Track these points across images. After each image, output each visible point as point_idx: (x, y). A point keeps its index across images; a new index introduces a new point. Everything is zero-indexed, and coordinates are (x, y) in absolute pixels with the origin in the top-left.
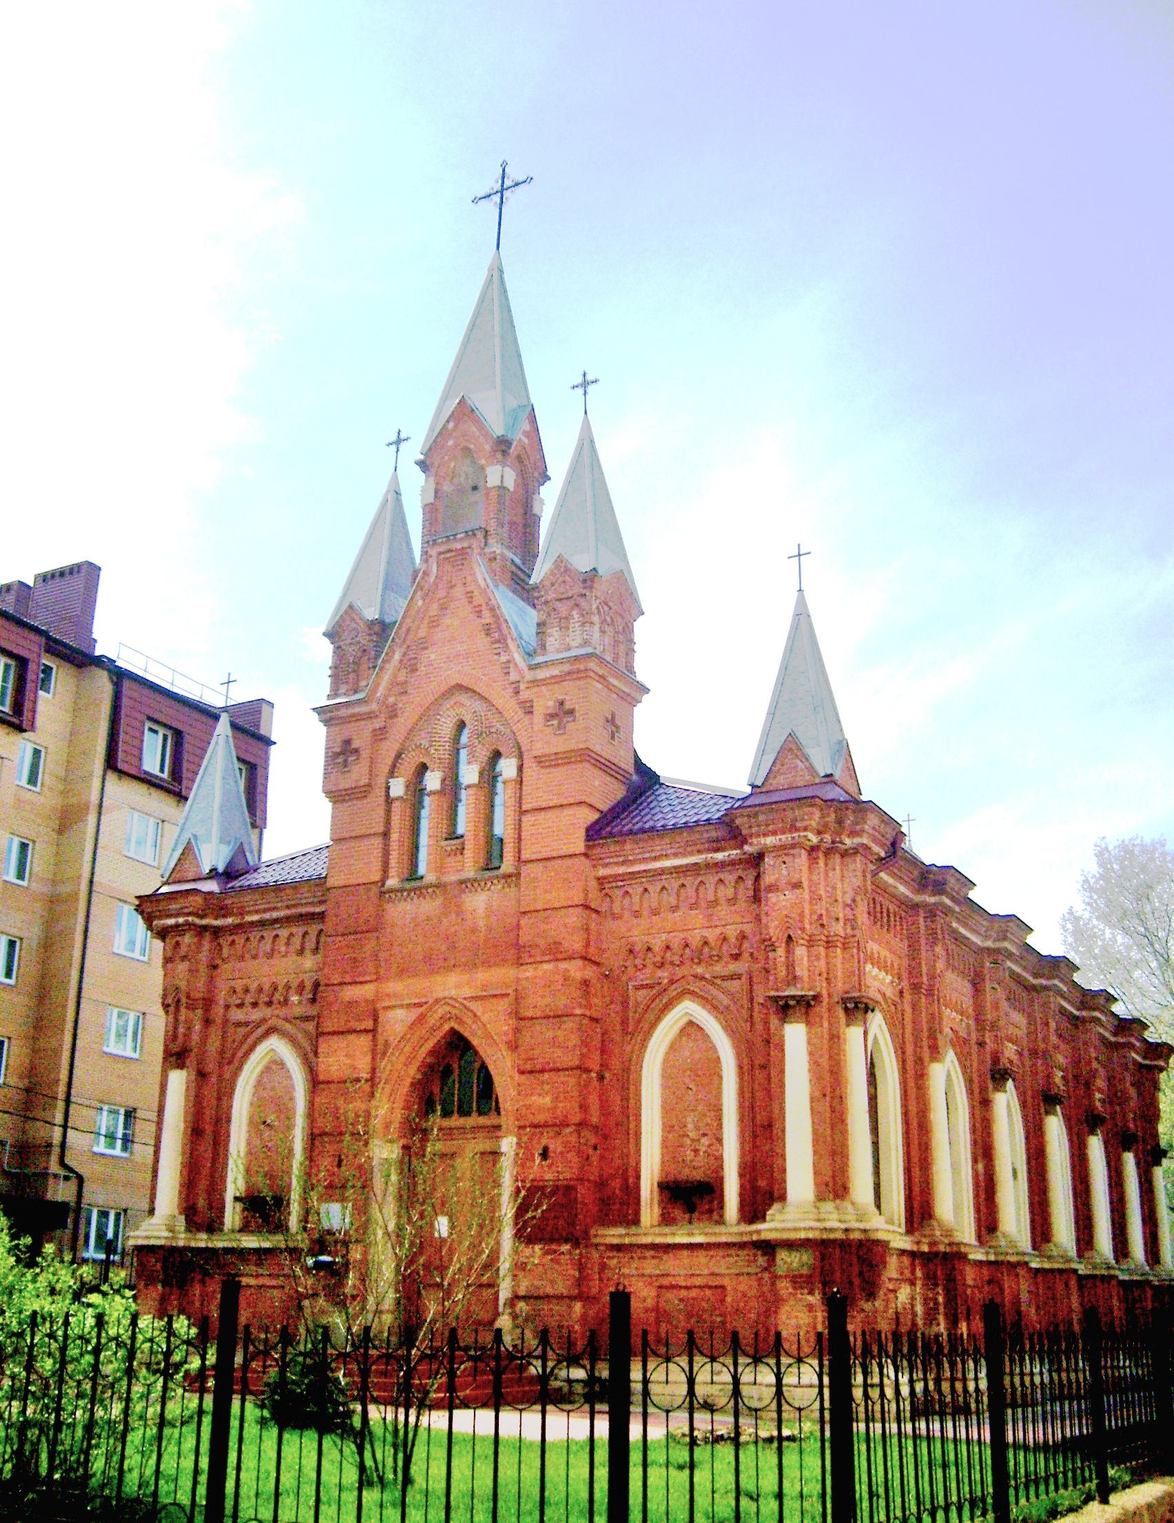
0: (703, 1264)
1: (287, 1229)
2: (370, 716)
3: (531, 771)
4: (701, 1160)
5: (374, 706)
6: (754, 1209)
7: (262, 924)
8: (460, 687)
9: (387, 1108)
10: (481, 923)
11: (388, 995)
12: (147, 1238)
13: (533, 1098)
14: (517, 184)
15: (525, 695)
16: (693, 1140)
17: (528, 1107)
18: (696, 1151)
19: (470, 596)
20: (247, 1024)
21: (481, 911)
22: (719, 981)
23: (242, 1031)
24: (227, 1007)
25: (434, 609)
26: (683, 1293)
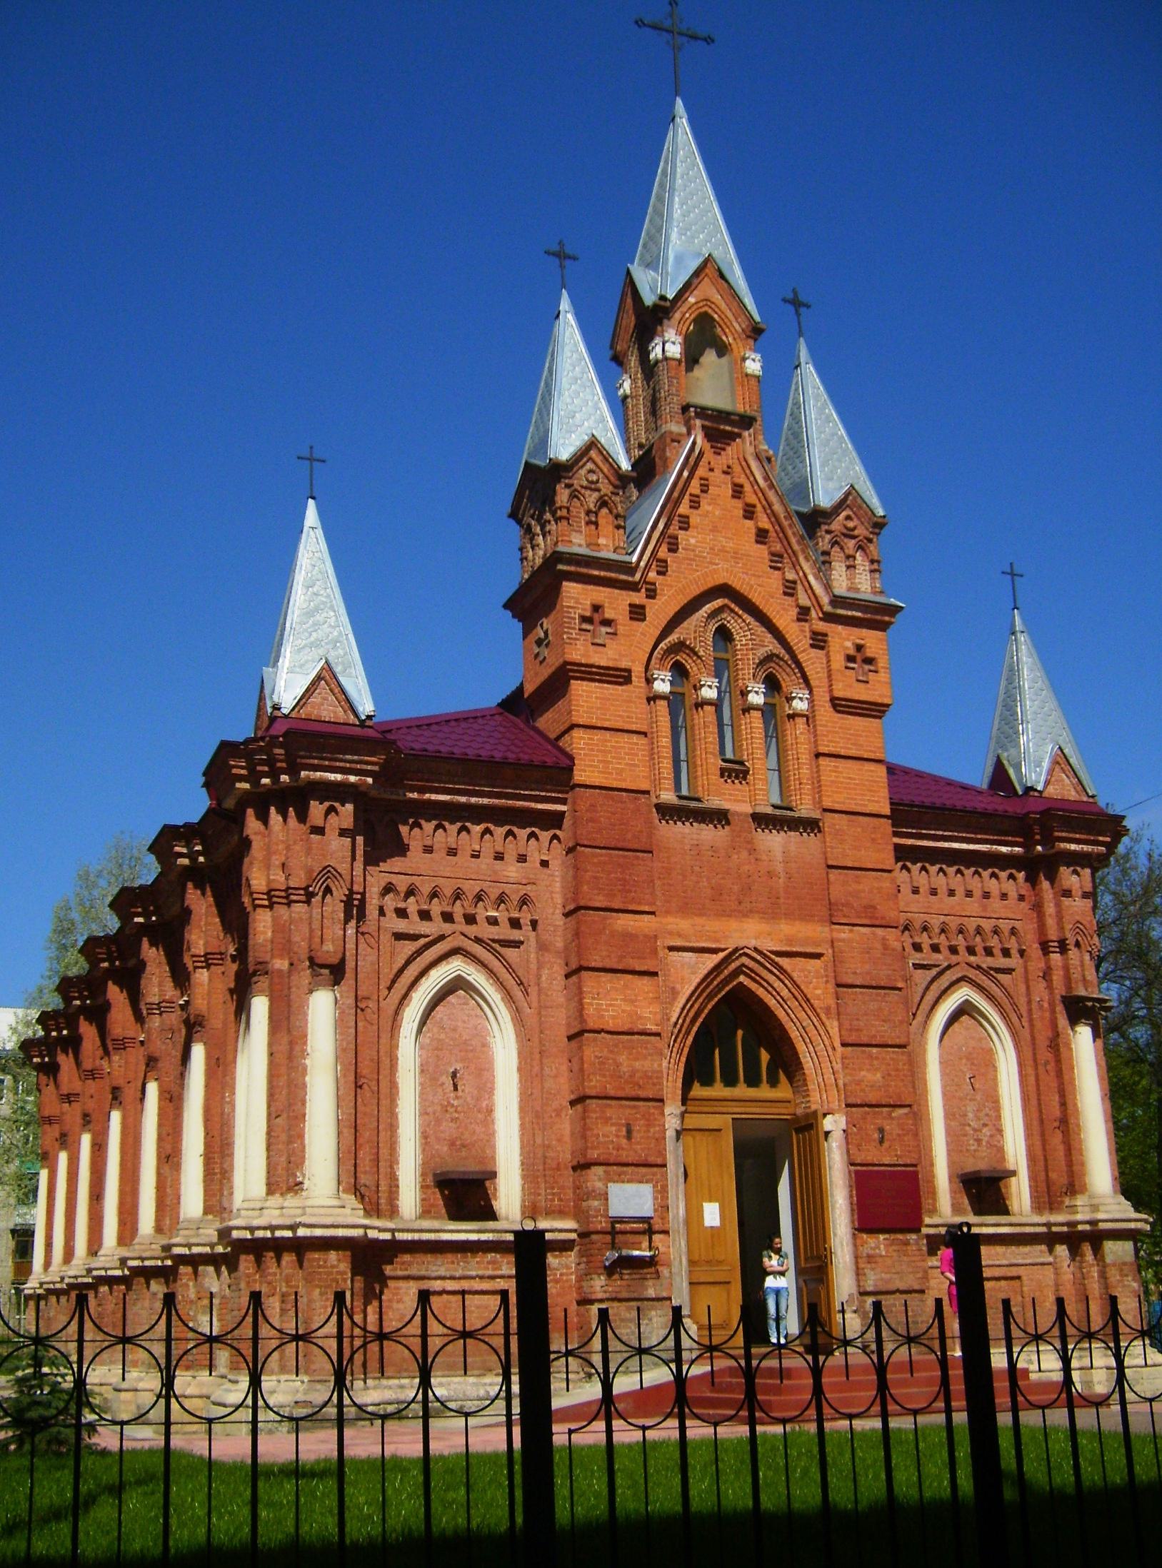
4: (984, 1152)
6: (1047, 1196)
10: (780, 868)
11: (671, 933)
13: (863, 1073)
15: (821, 626)
16: (975, 1130)
17: (858, 1083)
18: (979, 1141)
20: (415, 937)
21: (779, 856)
22: (496, 946)
23: (409, 947)
24: (382, 912)
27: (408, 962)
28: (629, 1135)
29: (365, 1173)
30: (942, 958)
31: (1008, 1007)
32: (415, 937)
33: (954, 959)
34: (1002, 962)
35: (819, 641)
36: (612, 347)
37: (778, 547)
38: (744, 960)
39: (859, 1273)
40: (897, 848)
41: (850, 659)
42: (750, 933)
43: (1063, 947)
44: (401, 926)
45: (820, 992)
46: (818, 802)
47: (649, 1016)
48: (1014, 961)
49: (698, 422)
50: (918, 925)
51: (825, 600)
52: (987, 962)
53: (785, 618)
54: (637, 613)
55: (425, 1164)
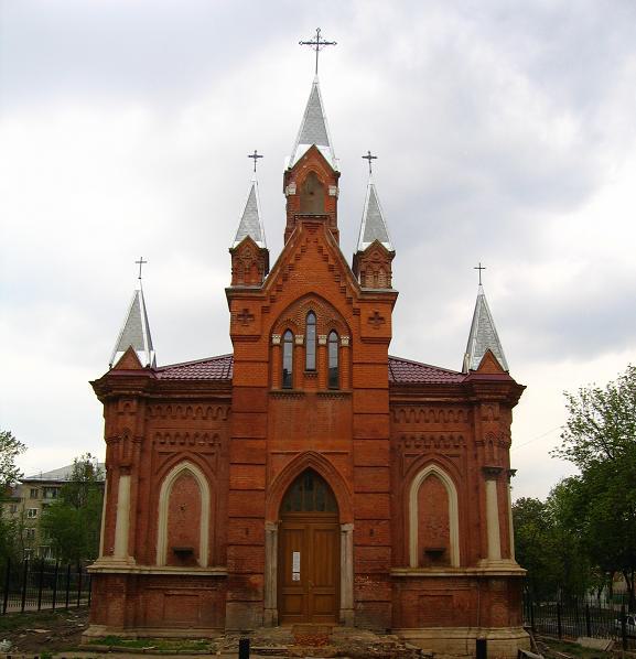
0: (441, 587)
1: (409, 565)
2: (262, 299)
3: (357, 345)
5: (265, 294)
6: (468, 560)
7: (183, 400)
8: (312, 294)
9: (271, 505)
12: (102, 569)
14: (327, 43)
15: (357, 306)
19: (320, 250)
20: (168, 453)
23: (165, 458)
24: (154, 443)
25: (298, 251)
26: (431, 599)
27: (164, 464)
28: (247, 533)
29: (142, 546)
30: (420, 451)
31: (456, 473)
32: (414, 456)
33: (428, 451)
34: (454, 452)
35: (357, 313)
36: (284, 192)
37: (338, 272)
38: (309, 457)
39: (355, 592)
40: (391, 403)
41: (371, 319)
42: (312, 445)
43: (483, 444)
44: (163, 449)
45: (344, 470)
46: (351, 385)
47: (260, 483)
48: (461, 451)
49: (300, 221)
50: (408, 437)
51: (358, 293)
52: (444, 452)
53: (341, 305)
54: (265, 310)
55: (169, 544)
